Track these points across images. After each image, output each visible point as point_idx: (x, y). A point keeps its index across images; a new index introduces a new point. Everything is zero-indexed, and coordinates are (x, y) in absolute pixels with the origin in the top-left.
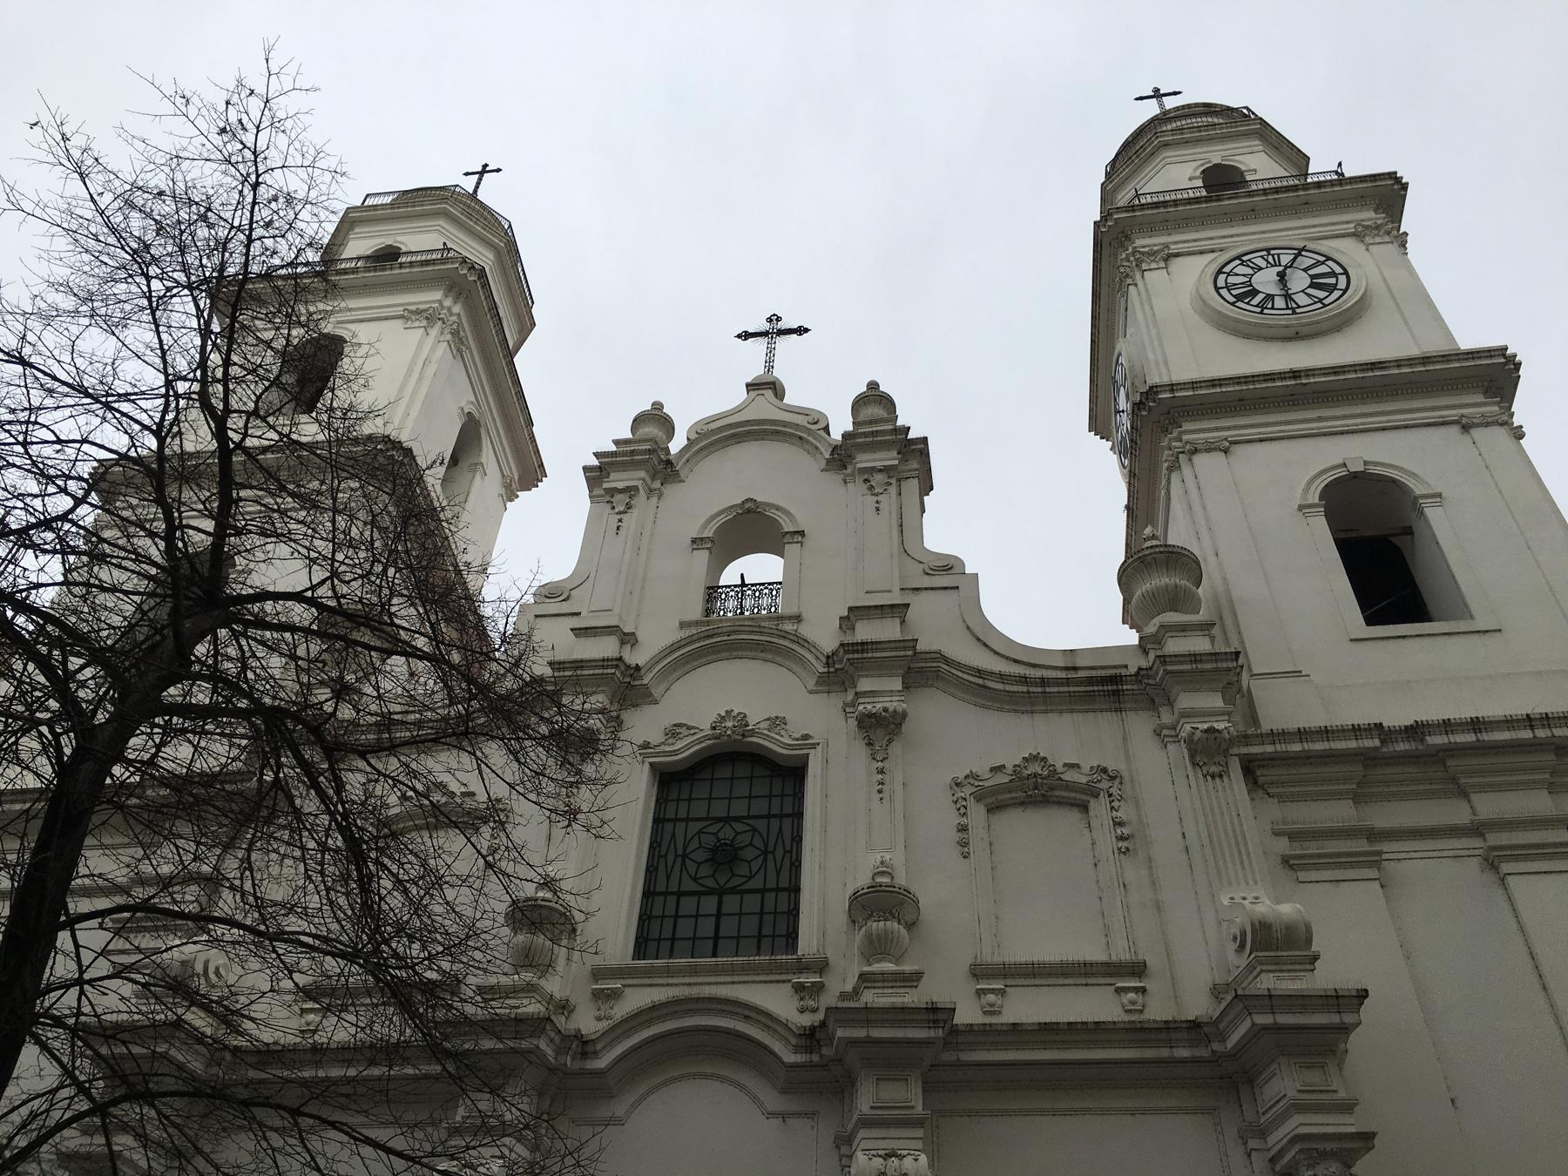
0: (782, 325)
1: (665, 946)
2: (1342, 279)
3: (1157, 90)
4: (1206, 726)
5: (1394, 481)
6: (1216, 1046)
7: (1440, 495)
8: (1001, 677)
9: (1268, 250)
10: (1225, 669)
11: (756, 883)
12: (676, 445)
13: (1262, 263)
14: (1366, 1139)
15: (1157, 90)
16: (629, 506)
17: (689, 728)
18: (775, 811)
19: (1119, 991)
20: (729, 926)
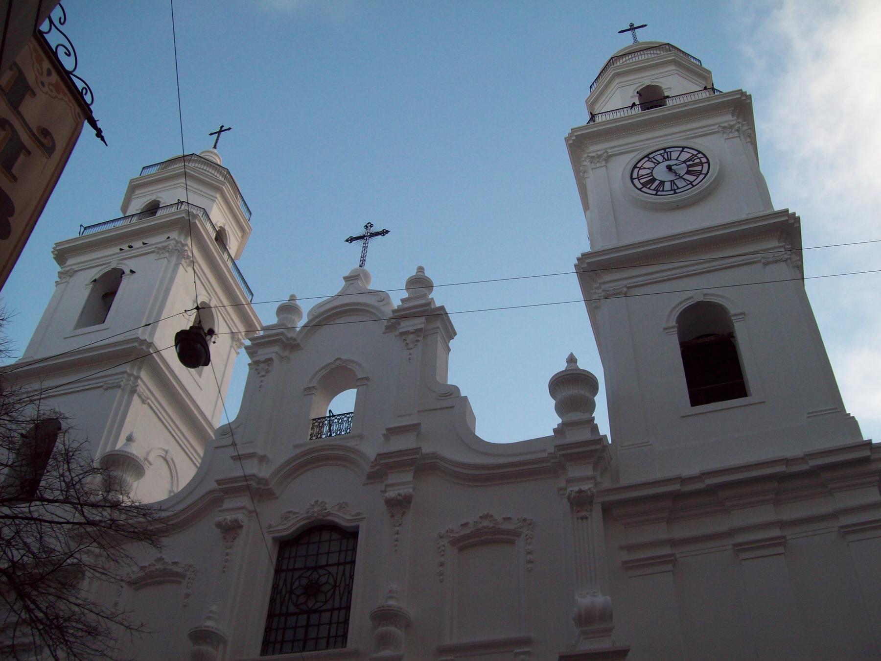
0: (373, 230)
1: (278, 646)
2: (706, 166)
3: (632, 25)
4: (576, 489)
11: (329, 606)
12: (302, 322)
13: (660, 158)
15: (632, 25)
16: (268, 371)
17: (295, 513)
19: (517, 654)
20: (312, 633)
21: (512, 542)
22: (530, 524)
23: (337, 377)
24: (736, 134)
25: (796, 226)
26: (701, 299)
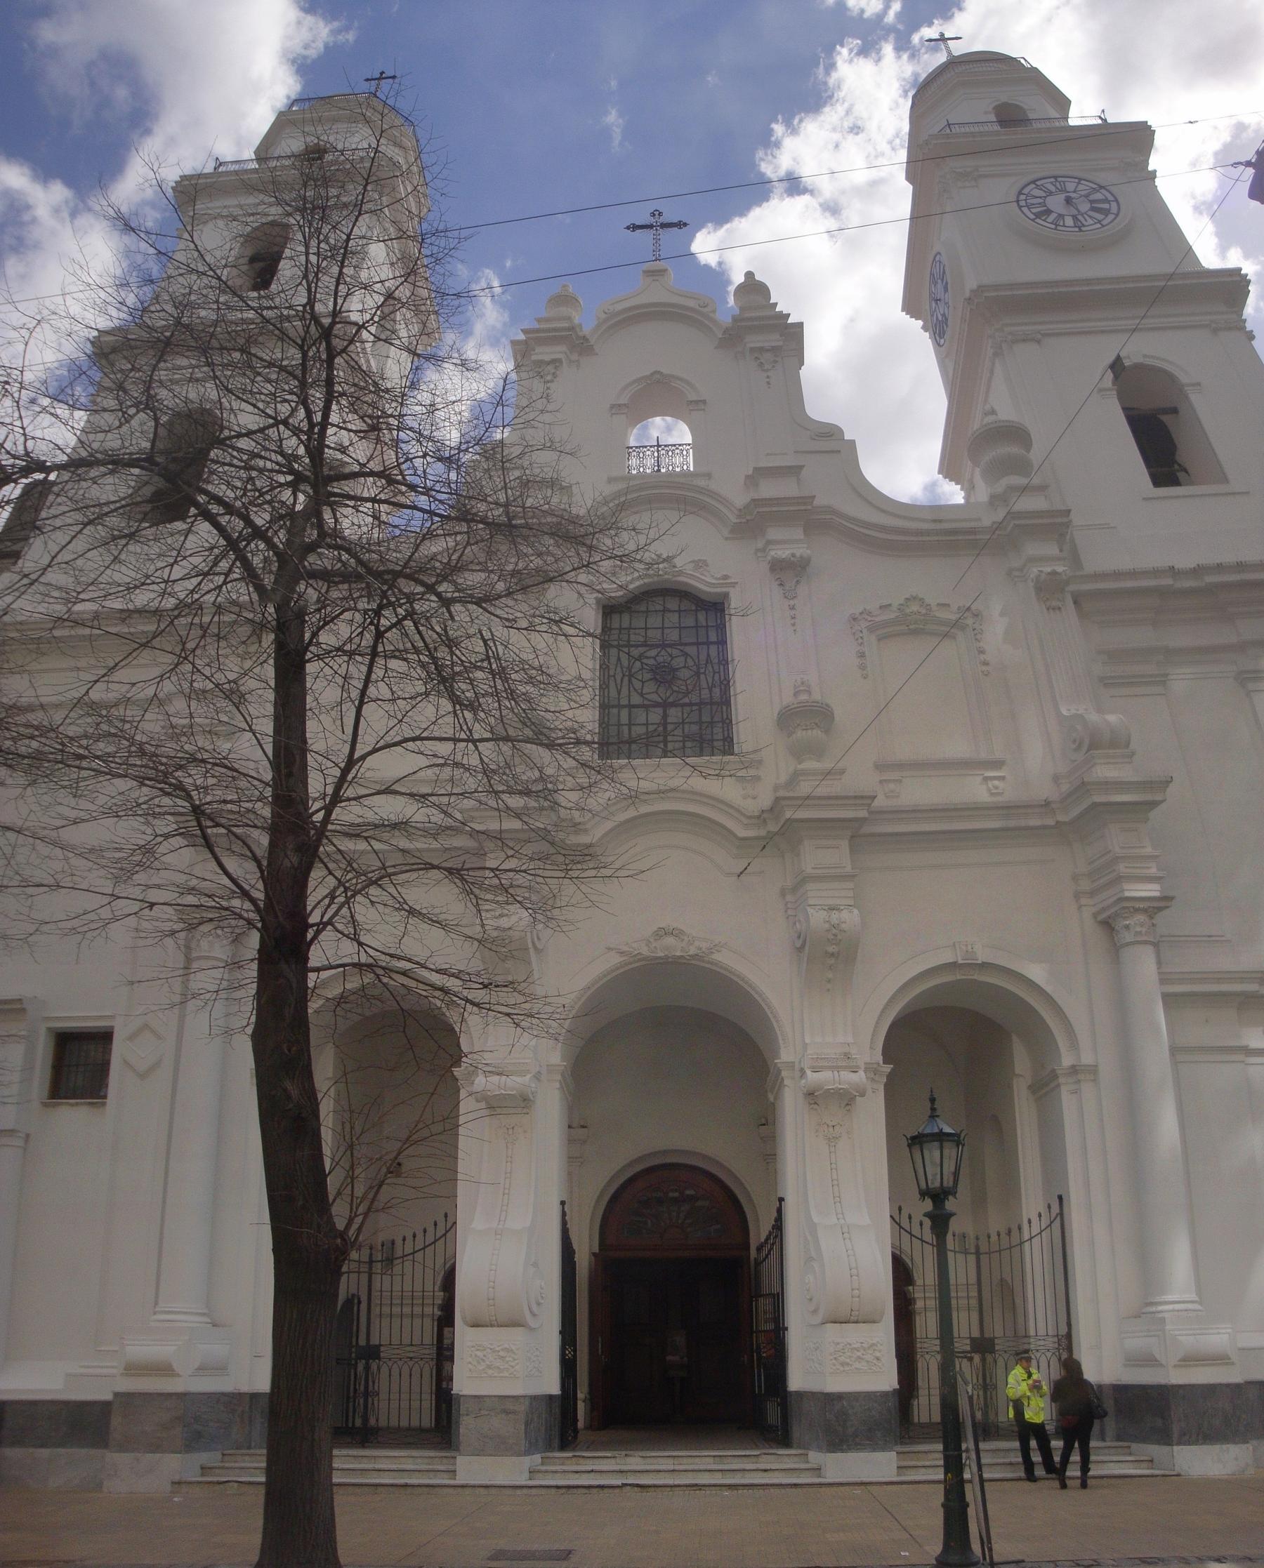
0: (666, 218)
4: (1049, 570)
5: (1165, 372)
7: (1199, 384)
8: (883, 529)
9: (1056, 177)
10: (1055, 525)
15: (942, 35)
18: (702, 639)
19: (986, 779)
23: (657, 394)
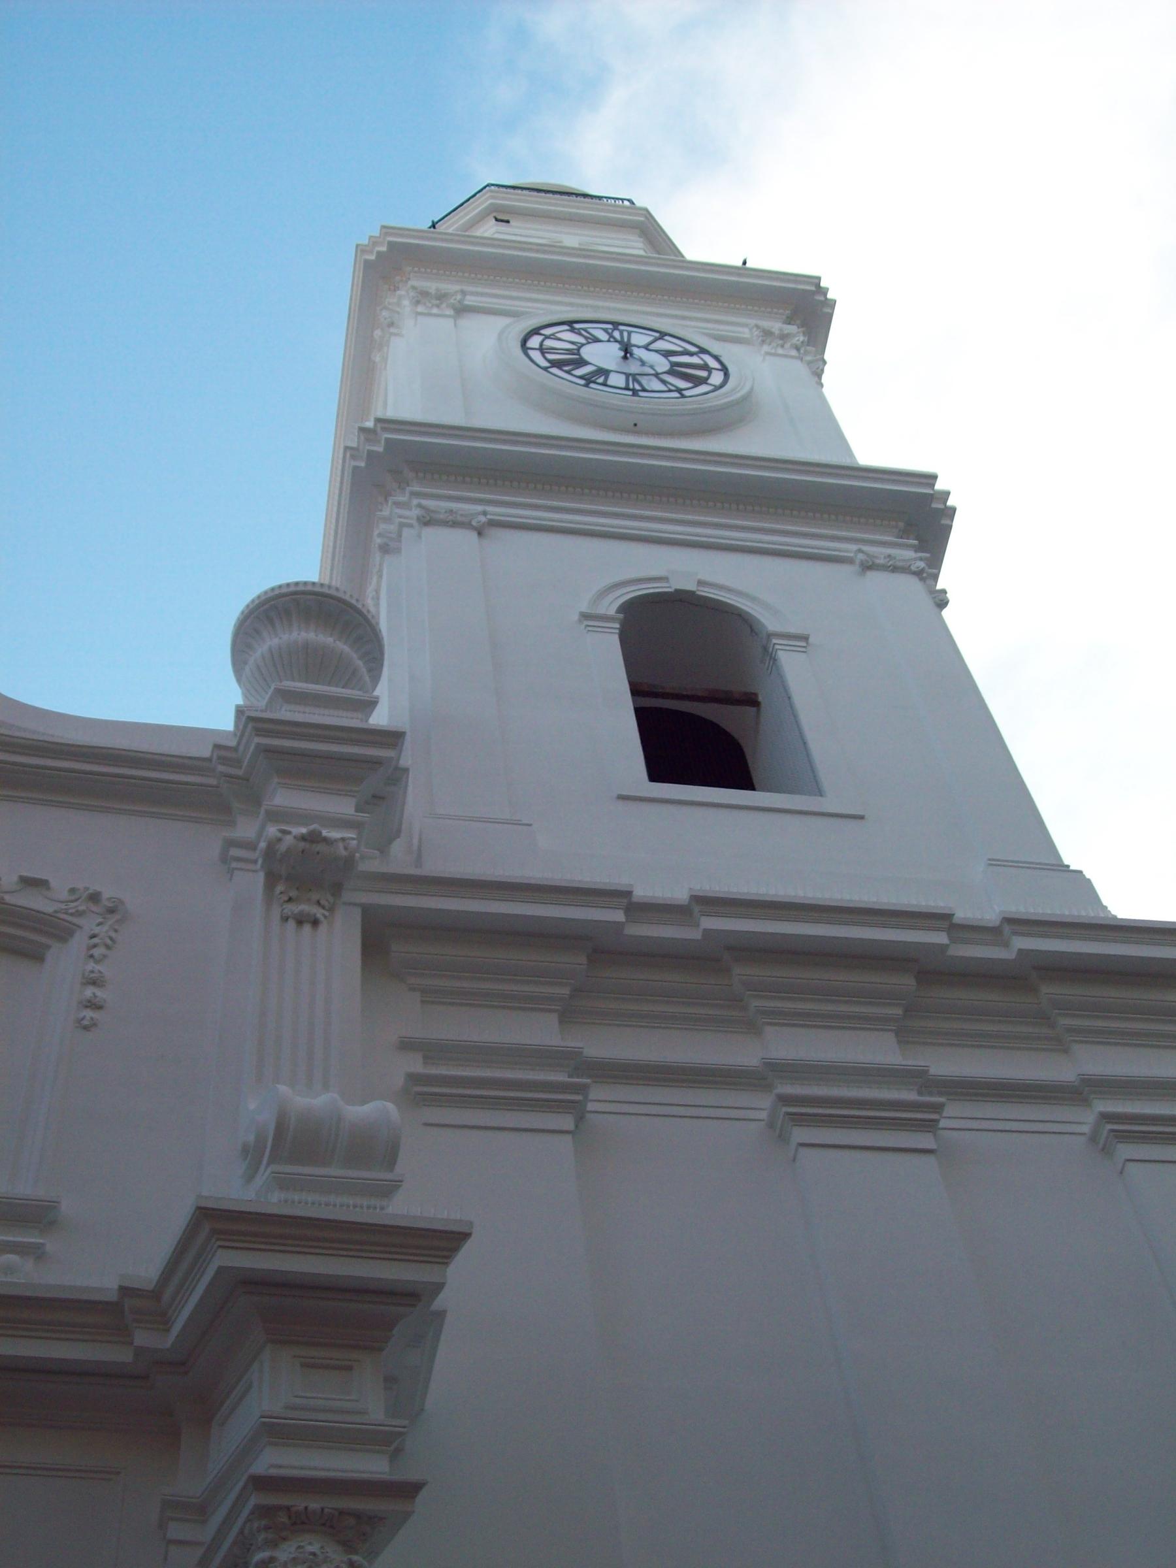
4: (304, 830)
6: (142, 1338)
7: (805, 638)
9: (616, 325)
13: (603, 336)
14: (409, 1490)
21: (36, 956)
22: (111, 911)
24: (794, 353)
25: (944, 522)
26: (690, 586)
